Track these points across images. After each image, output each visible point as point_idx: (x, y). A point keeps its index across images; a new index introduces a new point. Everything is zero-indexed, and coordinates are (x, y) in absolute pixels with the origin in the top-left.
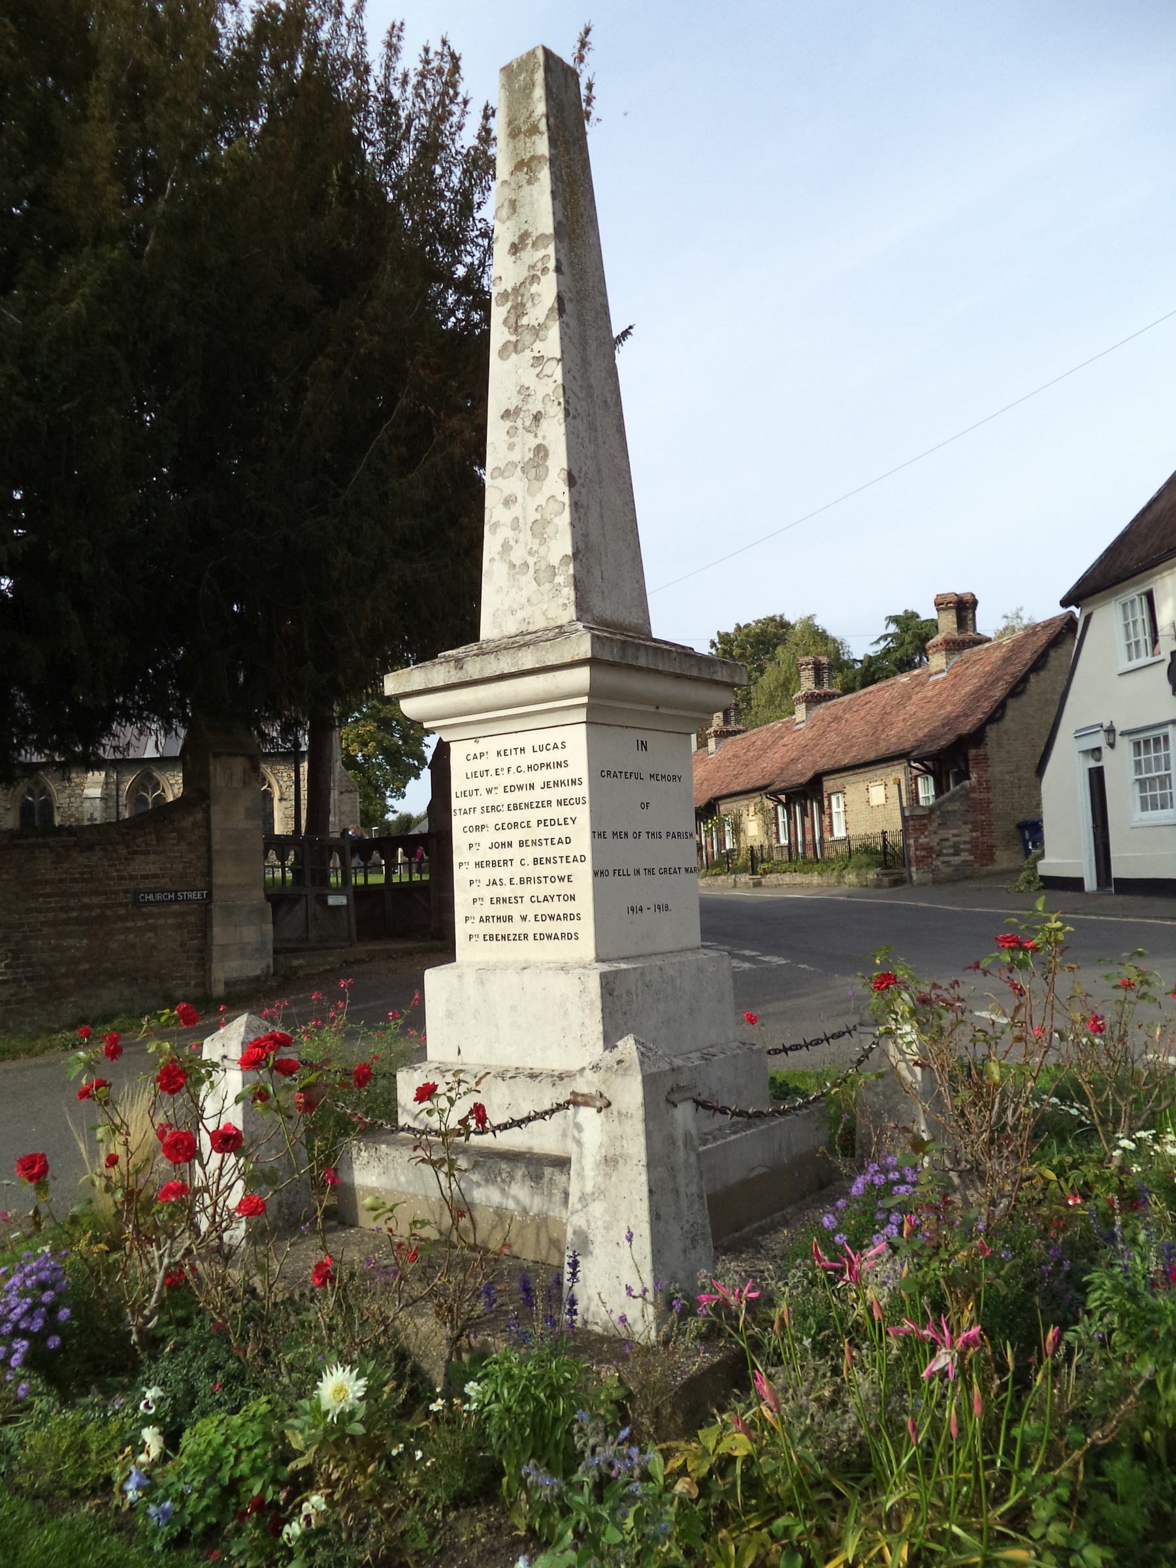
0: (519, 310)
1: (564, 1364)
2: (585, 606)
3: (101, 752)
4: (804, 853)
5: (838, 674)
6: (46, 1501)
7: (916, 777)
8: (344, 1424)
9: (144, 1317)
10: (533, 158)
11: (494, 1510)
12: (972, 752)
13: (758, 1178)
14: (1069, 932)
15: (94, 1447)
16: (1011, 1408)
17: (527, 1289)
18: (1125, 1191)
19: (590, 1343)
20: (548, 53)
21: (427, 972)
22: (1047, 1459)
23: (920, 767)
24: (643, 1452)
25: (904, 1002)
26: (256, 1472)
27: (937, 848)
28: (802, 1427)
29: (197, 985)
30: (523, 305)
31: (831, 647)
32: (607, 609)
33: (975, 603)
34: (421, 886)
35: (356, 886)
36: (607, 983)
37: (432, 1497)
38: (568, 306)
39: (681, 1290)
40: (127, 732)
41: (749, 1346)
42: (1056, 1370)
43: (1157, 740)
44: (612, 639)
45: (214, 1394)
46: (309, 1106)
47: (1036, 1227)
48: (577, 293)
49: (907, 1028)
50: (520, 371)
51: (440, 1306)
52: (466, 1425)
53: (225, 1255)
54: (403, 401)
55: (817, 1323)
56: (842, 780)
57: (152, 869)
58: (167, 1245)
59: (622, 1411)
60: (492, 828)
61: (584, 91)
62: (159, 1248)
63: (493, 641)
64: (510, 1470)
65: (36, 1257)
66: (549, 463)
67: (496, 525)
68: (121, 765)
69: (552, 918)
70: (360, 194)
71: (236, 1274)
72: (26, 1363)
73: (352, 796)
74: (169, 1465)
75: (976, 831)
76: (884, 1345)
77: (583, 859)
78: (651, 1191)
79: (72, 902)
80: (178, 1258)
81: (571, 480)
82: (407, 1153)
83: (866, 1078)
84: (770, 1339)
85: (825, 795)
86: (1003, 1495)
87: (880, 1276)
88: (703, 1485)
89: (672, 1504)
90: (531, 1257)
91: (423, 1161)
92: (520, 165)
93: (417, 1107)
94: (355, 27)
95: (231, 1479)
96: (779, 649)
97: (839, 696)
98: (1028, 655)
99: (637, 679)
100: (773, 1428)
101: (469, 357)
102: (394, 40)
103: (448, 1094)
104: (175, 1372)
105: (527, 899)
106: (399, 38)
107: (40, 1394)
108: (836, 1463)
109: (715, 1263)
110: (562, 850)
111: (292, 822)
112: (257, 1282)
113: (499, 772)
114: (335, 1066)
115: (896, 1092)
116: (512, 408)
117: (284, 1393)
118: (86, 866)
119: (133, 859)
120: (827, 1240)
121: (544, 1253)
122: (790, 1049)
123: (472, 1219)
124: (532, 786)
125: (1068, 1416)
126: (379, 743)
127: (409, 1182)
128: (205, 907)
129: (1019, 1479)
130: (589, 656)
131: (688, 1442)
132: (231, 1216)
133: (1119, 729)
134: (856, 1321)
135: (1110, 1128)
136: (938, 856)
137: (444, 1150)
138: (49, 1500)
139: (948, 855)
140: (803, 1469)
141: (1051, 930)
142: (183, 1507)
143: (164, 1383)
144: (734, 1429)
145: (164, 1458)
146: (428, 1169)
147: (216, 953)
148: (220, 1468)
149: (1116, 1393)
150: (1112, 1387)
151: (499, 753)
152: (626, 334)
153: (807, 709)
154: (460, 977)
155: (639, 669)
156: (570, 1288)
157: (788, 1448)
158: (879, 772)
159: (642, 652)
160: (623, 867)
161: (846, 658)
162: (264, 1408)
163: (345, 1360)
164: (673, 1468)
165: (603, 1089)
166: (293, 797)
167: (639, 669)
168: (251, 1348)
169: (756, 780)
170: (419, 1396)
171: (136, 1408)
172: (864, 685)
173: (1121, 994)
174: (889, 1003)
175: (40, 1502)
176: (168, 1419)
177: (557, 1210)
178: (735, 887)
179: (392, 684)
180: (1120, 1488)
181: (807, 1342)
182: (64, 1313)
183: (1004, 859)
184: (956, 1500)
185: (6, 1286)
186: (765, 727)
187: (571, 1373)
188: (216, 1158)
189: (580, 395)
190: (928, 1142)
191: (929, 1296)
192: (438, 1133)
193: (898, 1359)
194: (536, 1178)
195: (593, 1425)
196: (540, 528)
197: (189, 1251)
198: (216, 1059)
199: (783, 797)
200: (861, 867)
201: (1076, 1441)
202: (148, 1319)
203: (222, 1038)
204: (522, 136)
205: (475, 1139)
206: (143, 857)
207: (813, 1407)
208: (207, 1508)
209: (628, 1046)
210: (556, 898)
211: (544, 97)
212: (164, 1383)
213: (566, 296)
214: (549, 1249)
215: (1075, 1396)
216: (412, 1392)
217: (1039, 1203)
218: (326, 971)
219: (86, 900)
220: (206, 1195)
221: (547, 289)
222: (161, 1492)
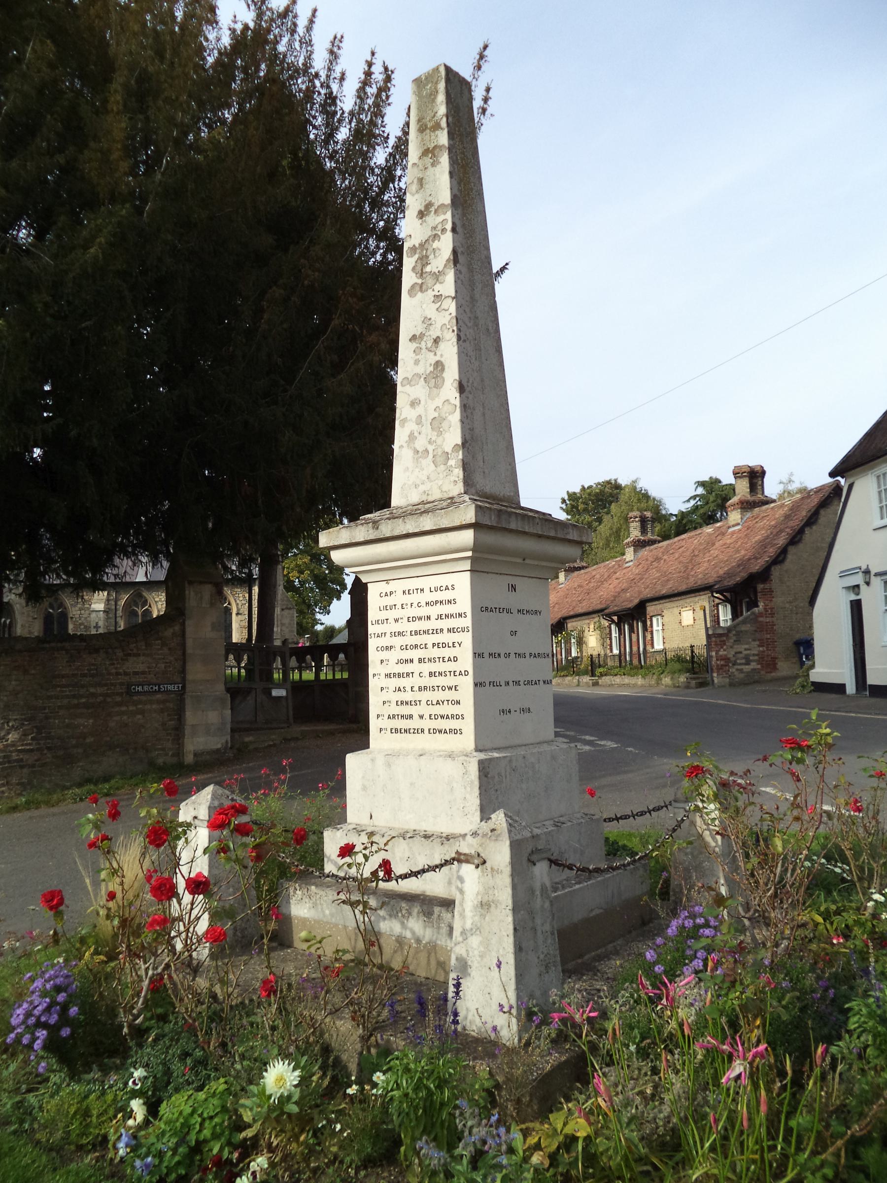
0: (424, 261)
1: (449, 1062)
2: (470, 483)
3: (105, 578)
4: (631, 660)
5: (660, 526)
6: (58, 1152)
7: (718, 604)
8: (283, 1104)
9: (133, 1015)
10: (435, 147)
11: (395, 1170)
12: (760, 587)
13: (598, 916)
14: (836, 736)
15: (95, 1112)
16: (789, 1104)
17: (422, 1003)
18: (876, 933)
19: (467, 1043)
20: (448, 69)
21: (348, 756)
22: (816, 1145)
23: (721, 597)
24: (508, 1131)
25: (708, 790)
26: (215, 1136)
27: (733, 659)
28: (629, 1115)
29: (173, 755)
30: (427, 257)
31: (651, 503)
32: (488, 485)
33: (763, 473)
34: (342, 682)
35: (294, 682)
36: (483, 768)
37: (348, 1160)
38: (461, 258)
39: (537, 1005)
40: (124, 564)
41: (588, 1049)
42: (823, 1077)
44: (490, 509)
45: (184, 1075)
46: (258, 858)
47: (809, 960)
48: (468, 247)
49: (712, 806)
50: (424, 306)
51: (355, 1012)
52: (374, 1106)
53: (195, 969)
54: (336, 322)
55: (641, 1034)
56: (661, 606)
57: (140, 667)
58: (152, 961)
59: (491, 1097)
60: (398, 648)
61: (477, 103)
62: (145, 963)
63: (401, 508)
64: (407, 1141)
65: (53, 965)
66: (445, 375)
67: (404, 421)
68: (120, 586)
69: (442, 717)
70: (311, 175)
71: (202, 983)
72: (45, 1047)
73: (291, 612)
74: (150, 1130)
75: (763, 646)
76: (691, 1051)
77: (466, 673)
78: (515, 929)
79: (82, 691)
80: (159, 970)
81: (462, 388)
82: (331, 894)
83: (679, 844)
84: (604, 1045)
85: (648, 617)
86: (782, 1172)
87: (689, 999)
88: (553, 1158)
89: (529, 1171)
90: (423, 974)
91: (344, 902)
92: (426, 152)
93: (341, 861)
94: (307, 43)
95: (197, 1141)
96: (613, 506)
97: (659, 542)
98: (804, 513)
99: (509, 538)
100: (606, 1114)
101: (385, 289)
102: (335, 49)
103: (364, 852)
104: (156, 1057)
105: (424, 702)
106: (339, 48)
107: (54, 1071)
108: (654, 1144)
109: (563, 983)
110: (451, 666)
111: (246, 631)
112: (217, 989)
113: (404, 606)
114: (278, 830)
115: (701, 853)
116: (418, 334)
117: (237, 1077)
118: (93, 665)
119: (127, 660)
120: (648, 970)
121: (433, 972)
122: (621, 818)
123: (380, 948)
124: (429, 618)
125: (832, 1112)
126: (312, 571)
127: (332, 915)
128: (181, 694)
129: (795, 1161)
130: (474, 521)
131: (542, 1123)
132: (199, 941)
133: (873, 571)
134: (670, 1032)
135: (866, 885)
136: (734, 665)
137: (361, 891)
138: (60, 1153)
139: (741, 664)
140: (629, 1147)
141: (821, 735)
142: (161, 1161)
143: (147, 1065)
144: (576, 1114)
145: (147, 1123)
146: (347, 908)
147: (188, 731)
148: (188, 1133)
149: (869, 1096)
150: (867, 1092)
151: (404, 592)
152: (503, 269)
153: (635, 551)
154: (373, 760)
155: (511, 531)
156: (455, 1004)
157: (618, 1131)
158: (688, 600)
159: (513, 518)
160: (497, 679)
161: (664, 512)
162: (222, 1087)
163: (285, 1055)
164: (530, 1144)
165: (480, 850)
166: (247, 613)
167: (511, 531)
168: (214, 1041)
169: (595, 603)
170: (338, 1083)
171: (126, 1084)
172: (678, 534)
173: (874, 782)
174: (698, 788)
175: (54, 1154)
176: (150, 1093)
177: (443, 940)
178: (578, 686)
179: (325, 539)
180: (872, 1170)
181: (633, 1048)
182: (74, 1010)
183: (785, 668)
184: (746, 1175)
185: (31, 988)
186: (603, 564)
187: (454, 1069)
188: (187, 898)
189: (469, 325)
190: (727, 899)
191: (727, 1016)
192: (355, 879)
193: (702, 1062)
194: (428, 914)
195: (471, 1111)
196: (437, 423)
197: (168, 966)
198: (189, 820)
199: (615, 618)
200: (675, 672)
201: (839, 1133)
202: (136, 1017)
203: (194, 803)
204: (428, 131)
205: (382, 885)
206: (135, 658)
207: (638, 1099)
208: (179, 1163)
209: (499, 818)
210: (446, 703)
211: (445, 101)
212: (147, 1065)
213: (459, 250)
214: (437, 969)
215: (838, 1097)
216: (334, 1079)
217: (810, 941)
218: (271, 746)
219: (92, 690)
220: (181, 923)
221: (445, 245)
222: (144, 1150)
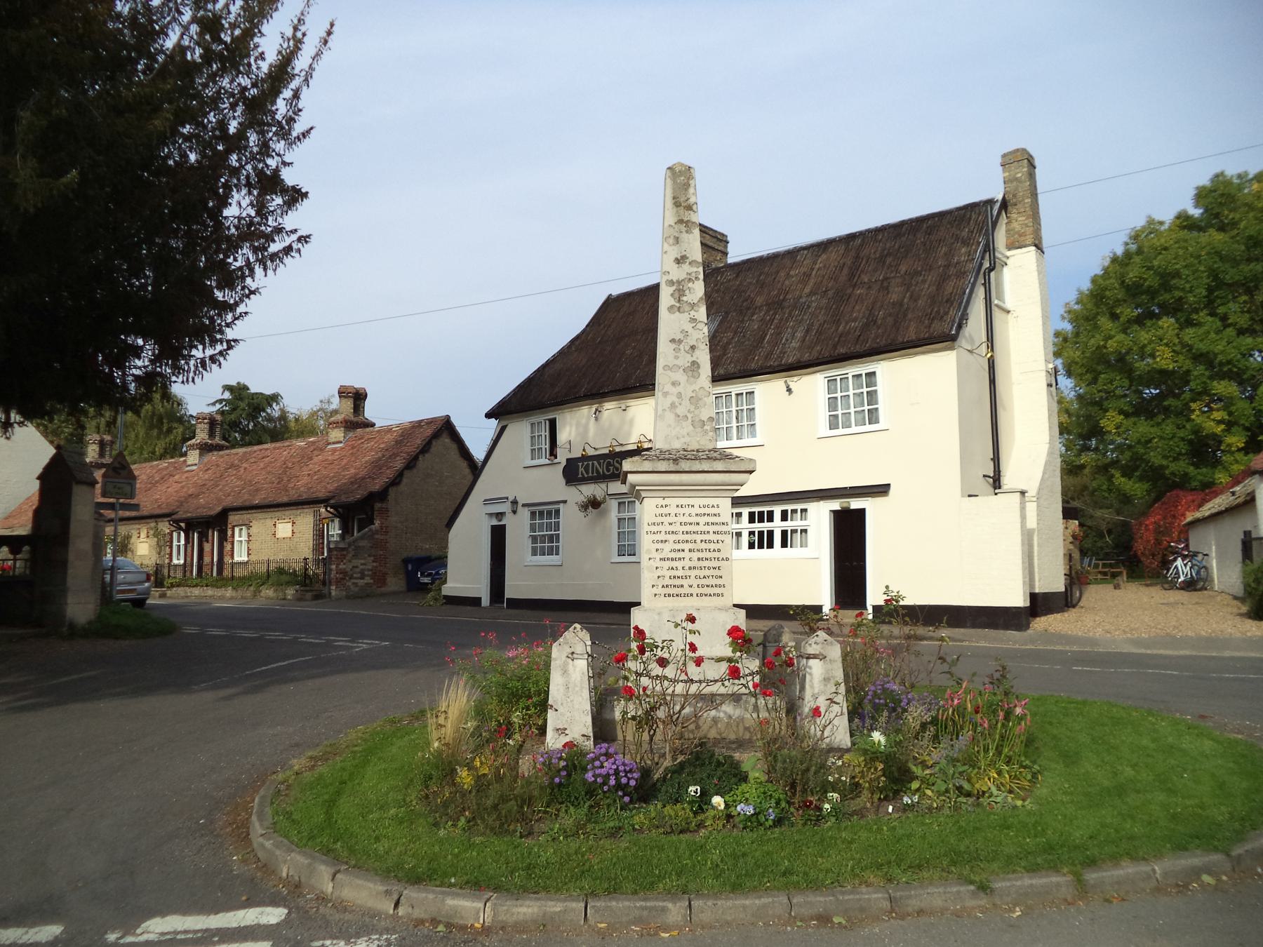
12: (378, 505)
43: (549, 513)
110: (716, 555)
133: (521, 502)
153: (201, 455)
158: (287, 513)
199: (183, 525)
